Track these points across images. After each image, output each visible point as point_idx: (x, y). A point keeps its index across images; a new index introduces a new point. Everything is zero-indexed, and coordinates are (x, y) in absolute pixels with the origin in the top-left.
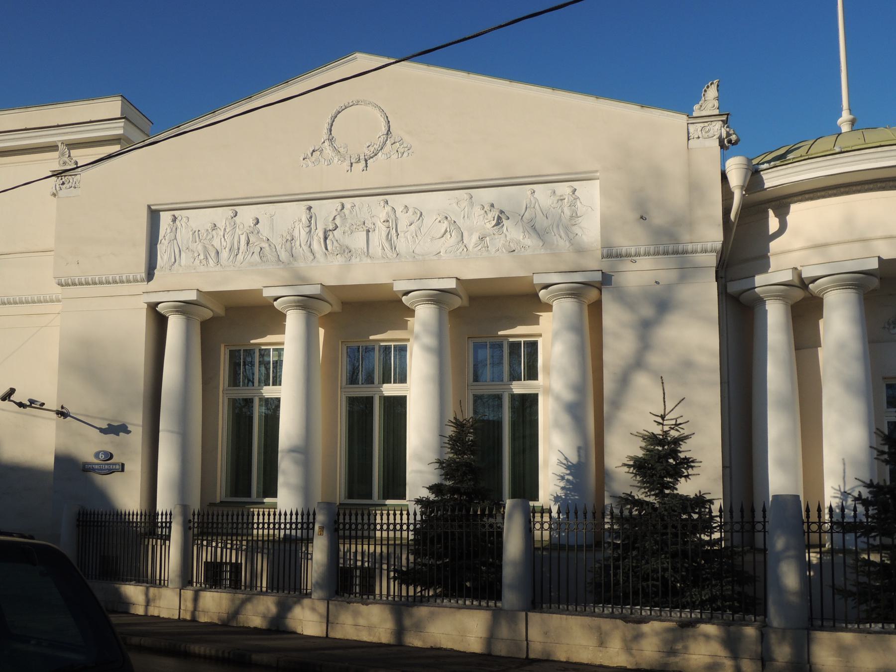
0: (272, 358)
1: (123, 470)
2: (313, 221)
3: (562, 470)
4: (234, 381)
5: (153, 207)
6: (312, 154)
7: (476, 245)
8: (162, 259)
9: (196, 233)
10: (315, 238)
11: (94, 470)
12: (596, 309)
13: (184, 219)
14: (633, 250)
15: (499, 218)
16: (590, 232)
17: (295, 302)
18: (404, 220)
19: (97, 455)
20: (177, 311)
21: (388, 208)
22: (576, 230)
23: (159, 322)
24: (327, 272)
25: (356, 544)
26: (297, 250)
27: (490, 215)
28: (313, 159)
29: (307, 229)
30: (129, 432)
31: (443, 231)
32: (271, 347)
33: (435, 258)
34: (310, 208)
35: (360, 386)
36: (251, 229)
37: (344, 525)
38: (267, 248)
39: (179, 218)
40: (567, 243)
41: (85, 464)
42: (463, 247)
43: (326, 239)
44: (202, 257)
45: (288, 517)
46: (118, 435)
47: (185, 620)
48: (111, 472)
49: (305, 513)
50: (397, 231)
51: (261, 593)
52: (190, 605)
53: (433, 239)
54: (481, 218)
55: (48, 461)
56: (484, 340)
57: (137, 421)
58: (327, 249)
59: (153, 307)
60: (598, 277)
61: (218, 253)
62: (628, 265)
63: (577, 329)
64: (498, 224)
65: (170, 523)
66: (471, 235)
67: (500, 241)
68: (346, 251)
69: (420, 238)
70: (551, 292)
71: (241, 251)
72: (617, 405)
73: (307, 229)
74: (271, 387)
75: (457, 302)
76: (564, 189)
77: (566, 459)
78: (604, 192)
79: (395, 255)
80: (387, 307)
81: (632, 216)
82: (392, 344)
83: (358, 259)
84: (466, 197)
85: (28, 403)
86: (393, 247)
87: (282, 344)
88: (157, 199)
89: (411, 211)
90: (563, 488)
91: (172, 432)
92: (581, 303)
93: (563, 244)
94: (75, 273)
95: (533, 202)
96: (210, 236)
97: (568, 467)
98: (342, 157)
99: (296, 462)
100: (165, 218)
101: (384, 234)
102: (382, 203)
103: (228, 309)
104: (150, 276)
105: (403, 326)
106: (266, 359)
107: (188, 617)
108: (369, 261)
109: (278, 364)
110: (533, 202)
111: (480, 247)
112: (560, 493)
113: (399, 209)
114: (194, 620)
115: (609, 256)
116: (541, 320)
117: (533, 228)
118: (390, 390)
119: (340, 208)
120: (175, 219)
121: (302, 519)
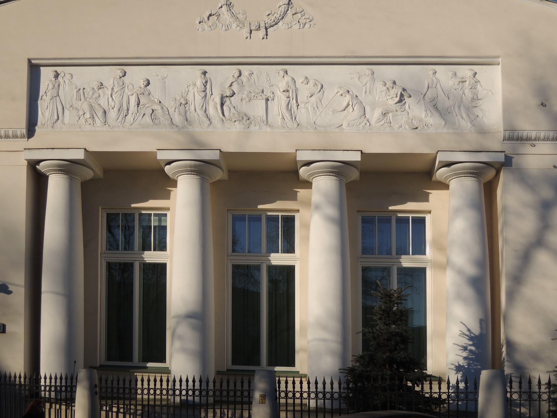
0: (154, 223)
2: (208, 86)
3: (465, 341)
4: (112, 245)
5: (33, 62)
6: (208, 19)
7: (379, 121)
8: (44, 113)
9: (81, 92)
10: (211, 103)
12: (488, 191)
13: (68, 76)
14: (533, 135)
15: (402, 95)
16: (493, 114)
17: (191, 166)
18: (304, 92)
21: (287, 78)
22: (477, 111)
23: (38, 181)
24: (227, 138)
25: (242, 410)
26: (191, 115)
27: (393, 92)
28: (210, 23)
29: (203, 94)
30: (10, 292)
31: (345, 104)
32: (152, 212)
33: (337, 130)
34: (205, 73)
35: (120, 252)
36: (142, 91)
37: (143, 390)
38: (160, 111)
39: (62, 74)
40: (469, 124)
42: (366, 121)
43: (222, 105)
44: (88, 115)
49: (69, 377)
50: (297, 101)
53: (334, 111)
54: (384, 93)
56: (372, 214)
58: (224, 115)
59: (33, 165)
60: (501, 158)
61: (105, 112)
62: (527, 149)
63: (475, 206)
64: (400, 101)
66: (373, 110)
67: (402, 119)
68: (246, 118)
69: (321, 109)
70: (454, 170)
71: (130, 112)
72: (518, 279)
73: (203, 94)
74: (152, 252)
75: (89, 174)
76: (465, 71)
77: (469, 330)
78: (506, 75)
79: (296, 125)
80: (285, 176)
81: (534, 102)
82: (280, 214)
83: (257, 127)
84: (368, 72)
86: (293, 118)
87: (168, 209)
88: (38, 53)
89: (311, 83)
90: (465, 358)
91: (57, 293)
92: (479, 182)
93: (465, 124)
95: (435, 82)
96: (96, 95)
97: (471, 339)
98: (241, 24)
99: (194, 328)
100: (46, 74)
101: (284, 104)
102: (282, 73)
103: (106, 171)
104: (31, 132)
105: (293, 197)
108: (268, 129)
109: (162, 230)
110: (435, 82)
111: (382, 122)
112: (462, 362)
113: (299, 81)
115: (511, 139)
116: (431, 197)
117: (435, 106)
119: (237, 74)
120: (57, 75)
121: (66, 383)
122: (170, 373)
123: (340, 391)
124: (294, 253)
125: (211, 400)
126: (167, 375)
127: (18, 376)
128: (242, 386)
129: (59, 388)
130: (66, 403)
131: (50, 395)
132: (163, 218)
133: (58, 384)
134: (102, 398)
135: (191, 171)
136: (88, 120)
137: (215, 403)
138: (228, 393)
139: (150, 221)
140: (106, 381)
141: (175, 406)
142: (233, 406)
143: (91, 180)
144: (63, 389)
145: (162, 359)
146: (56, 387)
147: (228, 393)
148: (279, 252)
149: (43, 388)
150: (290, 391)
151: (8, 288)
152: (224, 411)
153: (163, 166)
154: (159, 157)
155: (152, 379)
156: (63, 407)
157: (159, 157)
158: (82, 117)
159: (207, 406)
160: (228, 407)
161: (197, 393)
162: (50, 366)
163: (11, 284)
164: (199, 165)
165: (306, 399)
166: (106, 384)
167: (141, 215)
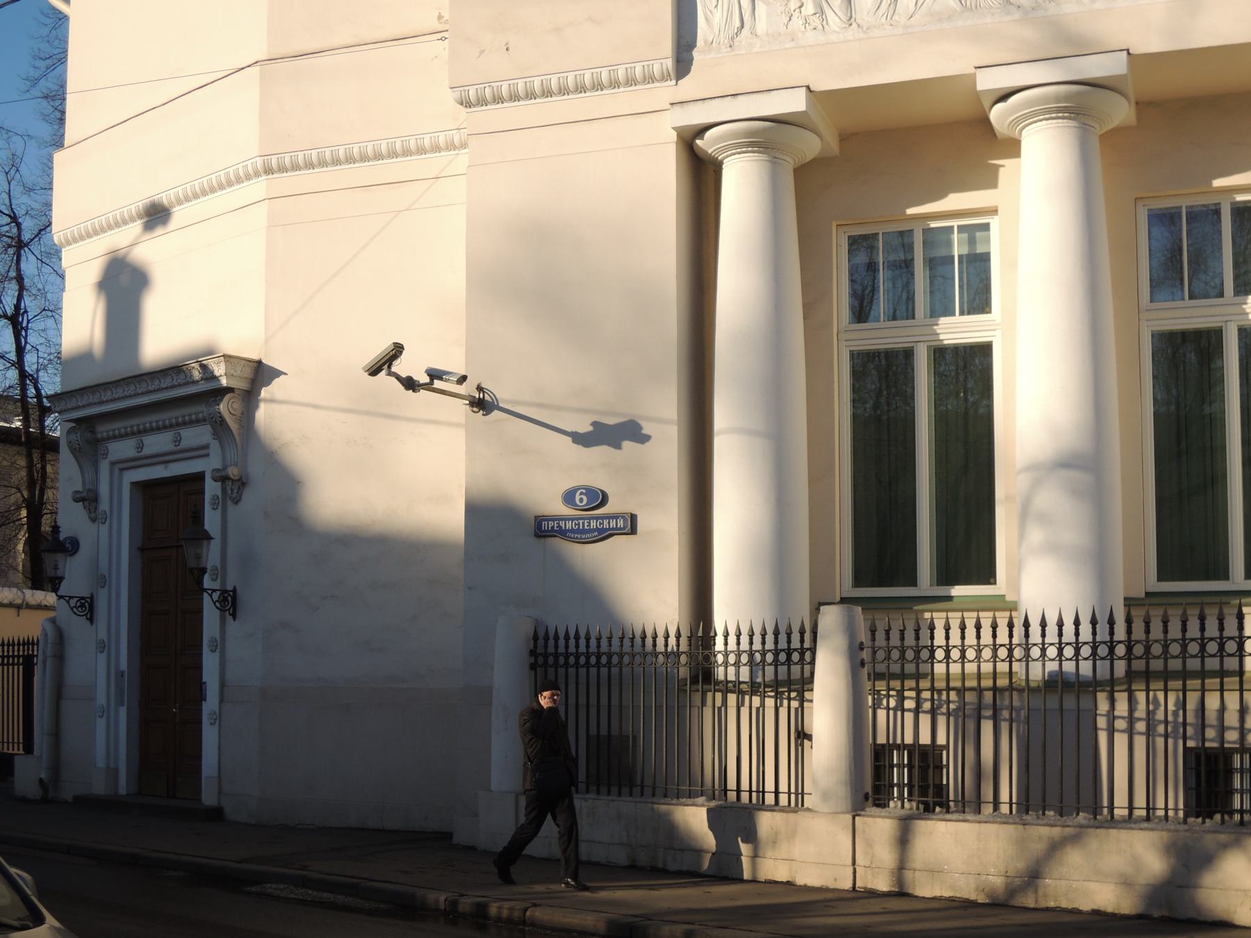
1: (633, 531)
11: (562, 533)
17: (1058, 99)
19: (569, 497)
20: (751, 144)
23: (701, 175)
25: (1203, 691)
32: (955, 223)
35: (881, 324)
37: (726, 655)
41: (539, 520)
45: (796, 637)
46: (618, 447)
47: (872, 894)
48: (604, 535)
49: (783, 630)
51: (1112, 822)
52: (886, 855)
55: (449, 519)
57: (664, 412)
59: (689, 140)
65: (813, 651)
74: (958, 318)
75: (810, 146)
85: (426, 379)
94: (499, 70)
103: (845, 138)
104: (683, 65)
106: (941, 252)
107: (883, 884)
109: (979, 264)
114: (901, 893)
118: (956, 329)
122: (1016, 609)
123: (1094, 639)
124: (914, 318)
125: (1120, 668)
126: (1007, 614)
127: (562, 635)
128: (1148, 631)
129: (758, 657)
130: (777, 693)
131: (738, 674)
132: (978, 234)
133: (757, 646)
134: (878, 676)
135: (1059, 110)
136: (810, 20)
137: (1131, 675)
138: (1166, 647)
139: (949, 244)
140: (887, 632)
141: (1029, 689)
142: (1178, 684)
143: (814, 162)
144: (770, 658)
145: (987, 574)
146: (751, 654)
147: (1166, 647)
148: (954, 314)
149: (720, 658)
150: (1138, 642)
151: (640, 428)
152: (1155, 697)
153: (986, 105)
154: (981, 86)
155: (970, 625)
156: (770, 702)
157: (981, 86)
158: (796, 14)
159: (1111, 685)
160: (1166, 685)
161: (1086, 651)
162: (736, 607)
163: (649, 419)
164: (1079, 94)
165: (1195, 656)
166: (888, 639)
167: (927, 231)
